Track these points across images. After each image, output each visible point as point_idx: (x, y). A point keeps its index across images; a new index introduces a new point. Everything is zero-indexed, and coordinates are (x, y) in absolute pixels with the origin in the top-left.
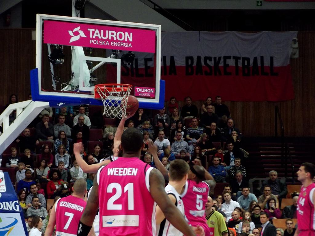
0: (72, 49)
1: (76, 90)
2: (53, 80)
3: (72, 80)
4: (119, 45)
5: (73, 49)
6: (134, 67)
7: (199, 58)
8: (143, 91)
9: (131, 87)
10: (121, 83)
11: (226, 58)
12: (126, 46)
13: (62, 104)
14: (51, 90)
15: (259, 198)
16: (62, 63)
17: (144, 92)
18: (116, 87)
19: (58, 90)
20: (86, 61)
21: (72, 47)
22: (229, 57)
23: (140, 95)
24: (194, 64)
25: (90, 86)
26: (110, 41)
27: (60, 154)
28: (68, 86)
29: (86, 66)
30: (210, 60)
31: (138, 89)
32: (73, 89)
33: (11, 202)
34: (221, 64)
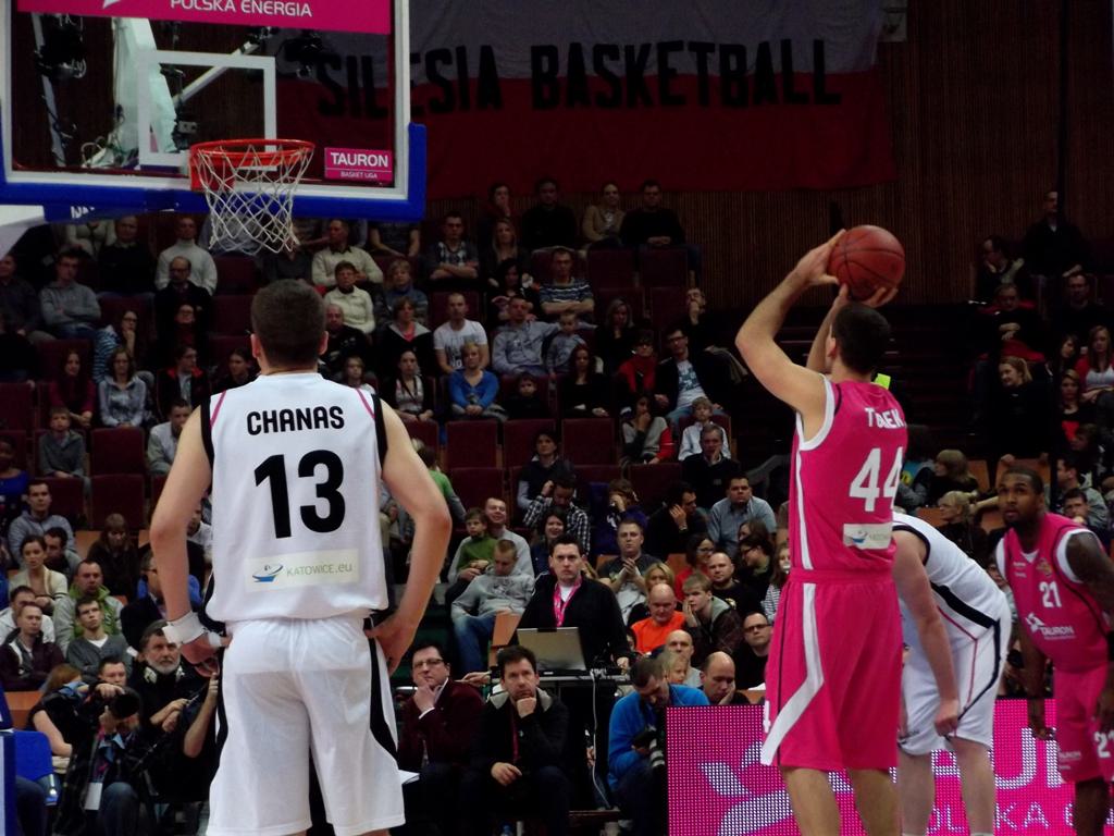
0: (114, 26)
1: (127, 163)
2: (54, 133)
3: (115, 132)
5: (118, 28)
6: (361, 83)
7: (576, 49)
8: (352, 160)
9: (307, 150)
10: (279, 136)
11: (665, 48)
12: (290, 11)
13: (85, 210)
14: (49, 165)
15: (781, 509)
16: (81, 75)
17: (356, 167)
18: (260, 148)
19: (74, 166)
20: (160, 68)
21: (116, 22)
22: (677, 46)
23: (343, 175)
24: (560, 71)
25: (174, 148)
27: (115, 380)
28: (103, 152)
29: (160, 84)
30: (614, 56)
31: (335, 155)
32: (119, 160)
34: (652, 70)
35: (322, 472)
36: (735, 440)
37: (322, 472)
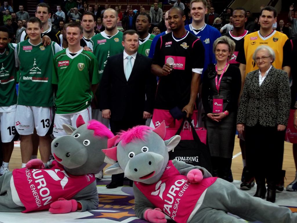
4: (34, 194)
12: (37, 202)
17: (63, 64)
26: (33, 182)
33: (194, 157)
35: (48, 121)
36: (228, 213)
37: (48, 121)
